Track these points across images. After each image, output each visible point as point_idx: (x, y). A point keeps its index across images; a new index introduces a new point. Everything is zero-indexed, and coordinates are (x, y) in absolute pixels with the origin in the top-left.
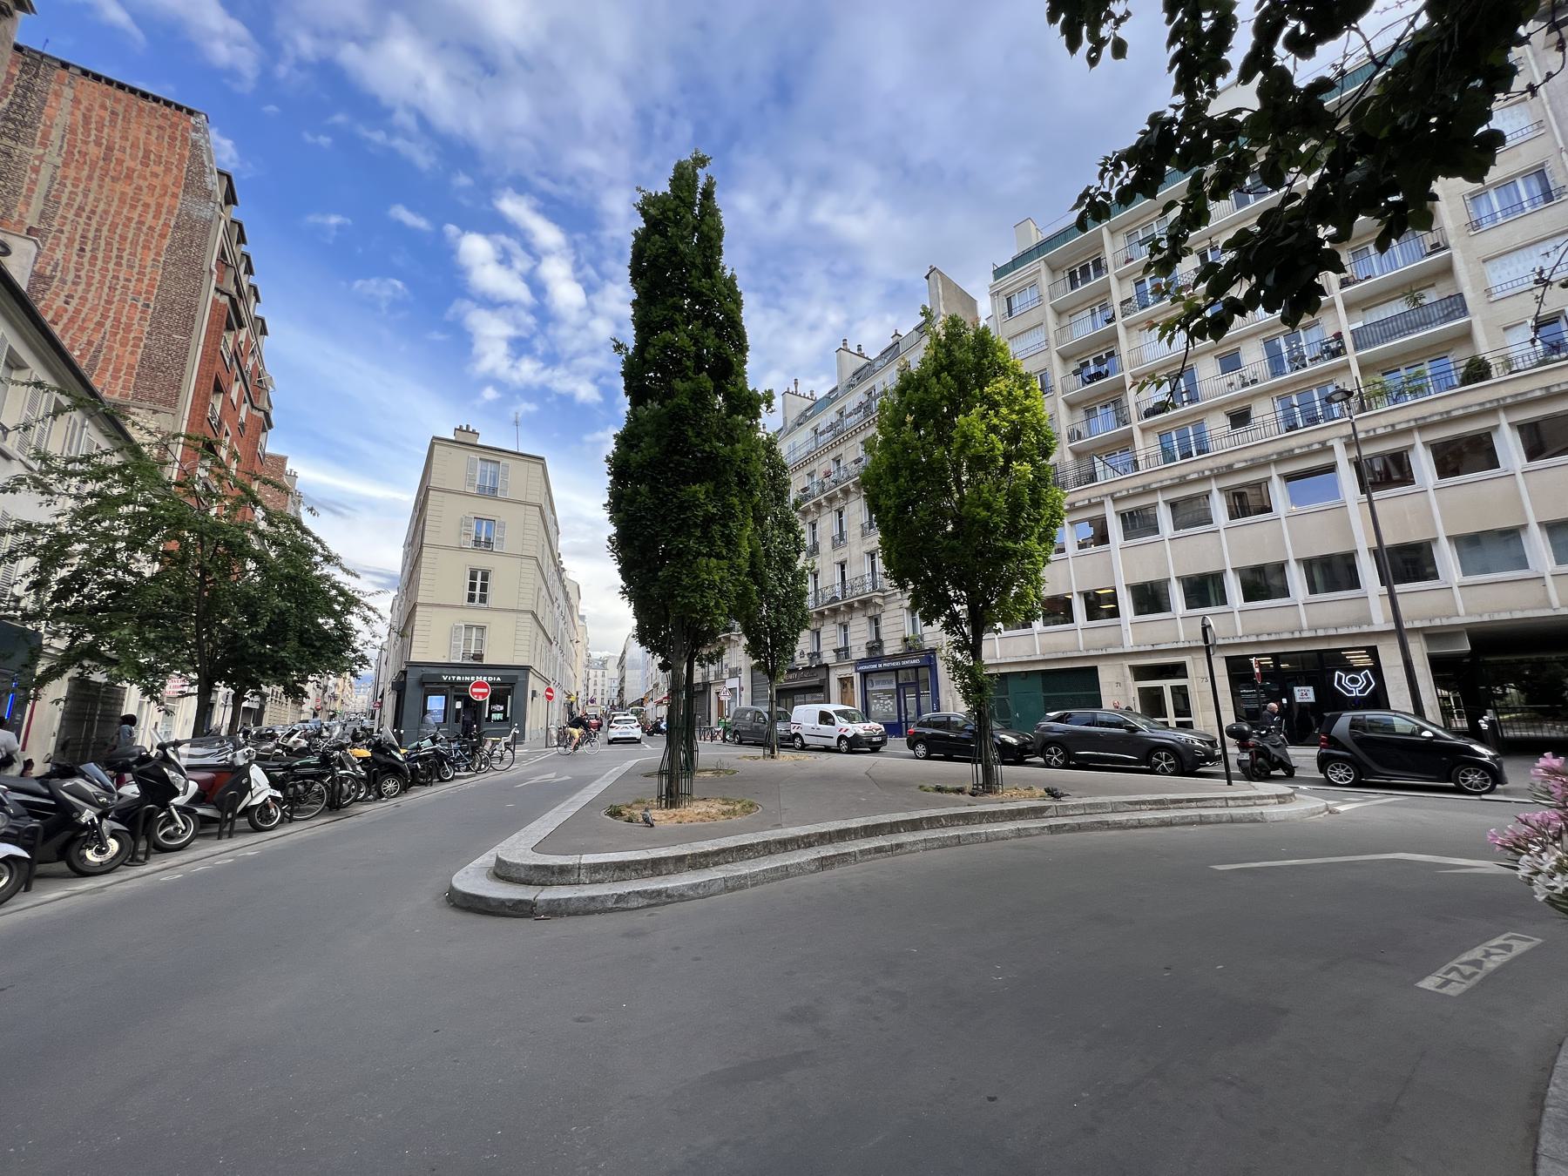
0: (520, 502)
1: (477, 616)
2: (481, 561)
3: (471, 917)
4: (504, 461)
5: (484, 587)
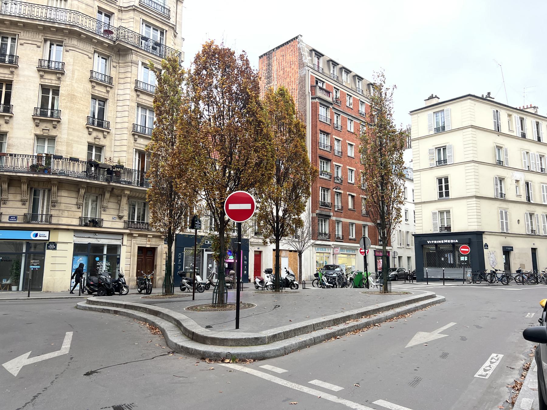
0: (459, 129)
1: (444, 205)
2: (442, 172)
3: (262, 361)
4: (445, 108)
5: (447, 187)
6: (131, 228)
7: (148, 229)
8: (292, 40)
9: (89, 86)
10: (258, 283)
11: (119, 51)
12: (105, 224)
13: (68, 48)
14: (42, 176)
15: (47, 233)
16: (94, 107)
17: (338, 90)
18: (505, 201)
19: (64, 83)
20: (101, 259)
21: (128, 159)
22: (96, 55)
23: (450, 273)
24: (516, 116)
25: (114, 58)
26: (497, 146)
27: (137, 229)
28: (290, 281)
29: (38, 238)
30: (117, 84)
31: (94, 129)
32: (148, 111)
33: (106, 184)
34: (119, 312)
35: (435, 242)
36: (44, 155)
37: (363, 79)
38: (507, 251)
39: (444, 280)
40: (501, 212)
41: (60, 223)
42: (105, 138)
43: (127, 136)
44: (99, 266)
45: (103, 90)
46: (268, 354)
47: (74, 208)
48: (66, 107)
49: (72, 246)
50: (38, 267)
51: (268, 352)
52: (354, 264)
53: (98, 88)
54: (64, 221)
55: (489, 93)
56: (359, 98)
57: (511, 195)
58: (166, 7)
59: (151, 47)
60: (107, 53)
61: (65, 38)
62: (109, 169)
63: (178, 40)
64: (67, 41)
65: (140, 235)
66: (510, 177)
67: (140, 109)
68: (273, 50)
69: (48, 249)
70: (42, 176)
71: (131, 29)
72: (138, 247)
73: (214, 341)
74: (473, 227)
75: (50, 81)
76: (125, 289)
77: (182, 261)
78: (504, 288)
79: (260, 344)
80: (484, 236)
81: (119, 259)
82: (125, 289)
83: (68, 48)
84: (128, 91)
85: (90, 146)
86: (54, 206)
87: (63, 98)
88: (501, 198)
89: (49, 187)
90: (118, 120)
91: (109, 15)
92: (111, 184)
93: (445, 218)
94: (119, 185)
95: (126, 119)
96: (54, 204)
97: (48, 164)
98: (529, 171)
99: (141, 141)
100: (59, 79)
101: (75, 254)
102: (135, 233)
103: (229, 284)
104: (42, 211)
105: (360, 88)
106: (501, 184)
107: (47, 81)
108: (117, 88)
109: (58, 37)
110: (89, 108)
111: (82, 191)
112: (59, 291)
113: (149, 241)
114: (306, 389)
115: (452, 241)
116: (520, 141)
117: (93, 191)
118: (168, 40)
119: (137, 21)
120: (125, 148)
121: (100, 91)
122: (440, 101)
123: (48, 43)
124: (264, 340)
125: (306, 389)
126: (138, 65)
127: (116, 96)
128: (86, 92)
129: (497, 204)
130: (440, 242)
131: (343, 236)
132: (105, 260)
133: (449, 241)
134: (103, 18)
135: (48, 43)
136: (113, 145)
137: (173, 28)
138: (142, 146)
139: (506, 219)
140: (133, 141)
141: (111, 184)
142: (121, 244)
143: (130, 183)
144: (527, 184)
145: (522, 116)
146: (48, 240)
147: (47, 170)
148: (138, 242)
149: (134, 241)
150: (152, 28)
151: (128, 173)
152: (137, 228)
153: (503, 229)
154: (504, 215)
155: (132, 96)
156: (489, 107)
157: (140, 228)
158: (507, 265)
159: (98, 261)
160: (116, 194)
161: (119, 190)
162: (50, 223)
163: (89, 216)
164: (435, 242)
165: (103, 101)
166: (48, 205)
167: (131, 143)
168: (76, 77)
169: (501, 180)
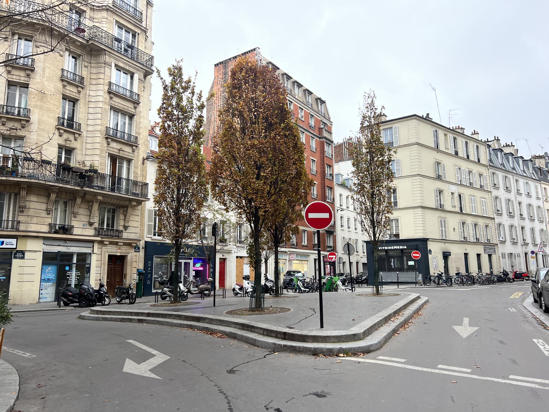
0: (406, 146)
4: (394, 126)
6: (102, 235)
7: (118, 236)
8: (249, 51)
9: (60, 85)
10: (237, 290)
11: (91, 51)
12: (76, 231)
13: (39, 44)
14: (12, 179)
15: (14, 241)
16: (64, 108)
17: (292, 102)
18: (444, 211)
19: (34, 80)
20: (71, 269)
21: (101, 163)
22: (67, 53)
23: (404, 276)
24: (450, 136)
25: (86, 57)
26: (437, 162)
27: (107, 236)
28: (269, 287)
29: (4, 246)
30: (88, 84)
31: (65, 131)
32: (120, 115)
33: (79, 188)
34: (145, 320)
35: (386, 248)
36: (10, 156)
37: (312, 93)
38: (446, 256)
39: (398, 283)
40: (441, 221)
41: (29, 230)
42: (76, 140)
43: (99, 139)
44: (69, 276)
45: (75, 90)
46: (371, 348)
47: (44, 214)
48: (36, 106)
49: (41, 254)
50: (4, 278)
51: (371, 346)
52: (306, 270)
53: (69, 87)
54: (33, 227)
55: (428, 114)
56: (309, 112)
57: (448, 206)
58: (137, 9)
59: (123, 49)
60: (79, 52)
61: (35, 33)
62: (81, 173)
63: (148, 44)
64: (38, 37)
65: (111, 243)
66: (448, 189)
67: (112, 112)
68: (230, 59)
69: (15, 258)
70: (12, 179)
71: (105, 29)
72: (109, 255)
73: (325, 339)
74: (419, 235)
75: (18, 78)
76: (107, 299)
77: (152, 270)
78: (450, 289)
79: (358, 340)
80: (428, 242)
81: (89, 268)
82: (107, 299)
83: (39, 44)
84: (101, 93)
85: (60, 147)
86: (23, 211)
87: (33, 96)
88: (440, 208)
89: (16, 191)
90: (90, 122)
91: (80, 13)
92: (85, 189)
93: (394, 226)
94: (92, 190)
95: (99, 122)
96: (22, 209)
97: (15, 166)
98: (461, 185)
99: (114, 145)
100: (28, 76)
101: (44, 264)
102: (106, 241)
103: (207, 292)
104: (8, 217)
105: (310, 102)
106: (440, 196)
107: (14, 77)
108: (88, 89)
109: (28, 32)
110: (57, 108)
111: (53, 196)
112: (27, 303)
113: (120, 249)
114: (437, 371)
115: (401, 247)
116: (454, 158)
117: (64, 196)
118: (140, 43)
119: (110, 21)
120: (98, 152)
121: (71, 91)
122: (388, 119)
123: (16, 37)
124: (360, 336)
125: (437, 371)
126: (111, 66)
127: (87, 97)
128: (57, 91)
129: (438, 214)
130: (390, 248)
131: (297, 243)
132: (74, 269)
133: (398, 247)
134: (74, 16)
135: (16, 37)
136: (84, 148)
137: (145, 31)
138: (115, 150)
139: (445, 228)
140: (106, 145)
141: (85, 189)
142: (91, 252)
143: (102, 188)
144: (460, 196)
145: (455, 136)
146: (16, 249)
147: (14, 172)
148: (108, 250)
149: (104, 249)
150: (124, 30)
151: (101, 177)
152: (108, 235)
153: (442, 236)
154: (443, 223)
155: (106, 98)
156: (430, 126)
157: (110, 235)
158: (446, 267)
159: (68, 271)
160: (88, 200)
161: (91, 195)
162: (18, 230)
163: (58, 223)
164: (386, 248)
165: (74, 102)
166: (14, 211)
167: (104, 147)
168: (46, 74)
169: (440, 192)
